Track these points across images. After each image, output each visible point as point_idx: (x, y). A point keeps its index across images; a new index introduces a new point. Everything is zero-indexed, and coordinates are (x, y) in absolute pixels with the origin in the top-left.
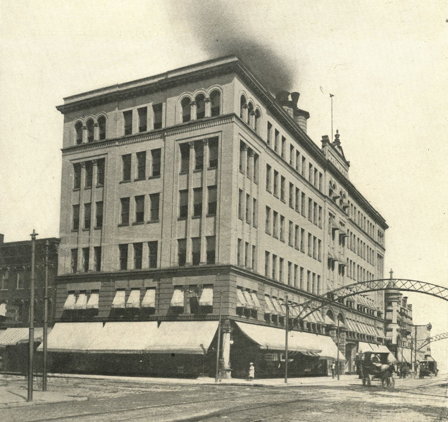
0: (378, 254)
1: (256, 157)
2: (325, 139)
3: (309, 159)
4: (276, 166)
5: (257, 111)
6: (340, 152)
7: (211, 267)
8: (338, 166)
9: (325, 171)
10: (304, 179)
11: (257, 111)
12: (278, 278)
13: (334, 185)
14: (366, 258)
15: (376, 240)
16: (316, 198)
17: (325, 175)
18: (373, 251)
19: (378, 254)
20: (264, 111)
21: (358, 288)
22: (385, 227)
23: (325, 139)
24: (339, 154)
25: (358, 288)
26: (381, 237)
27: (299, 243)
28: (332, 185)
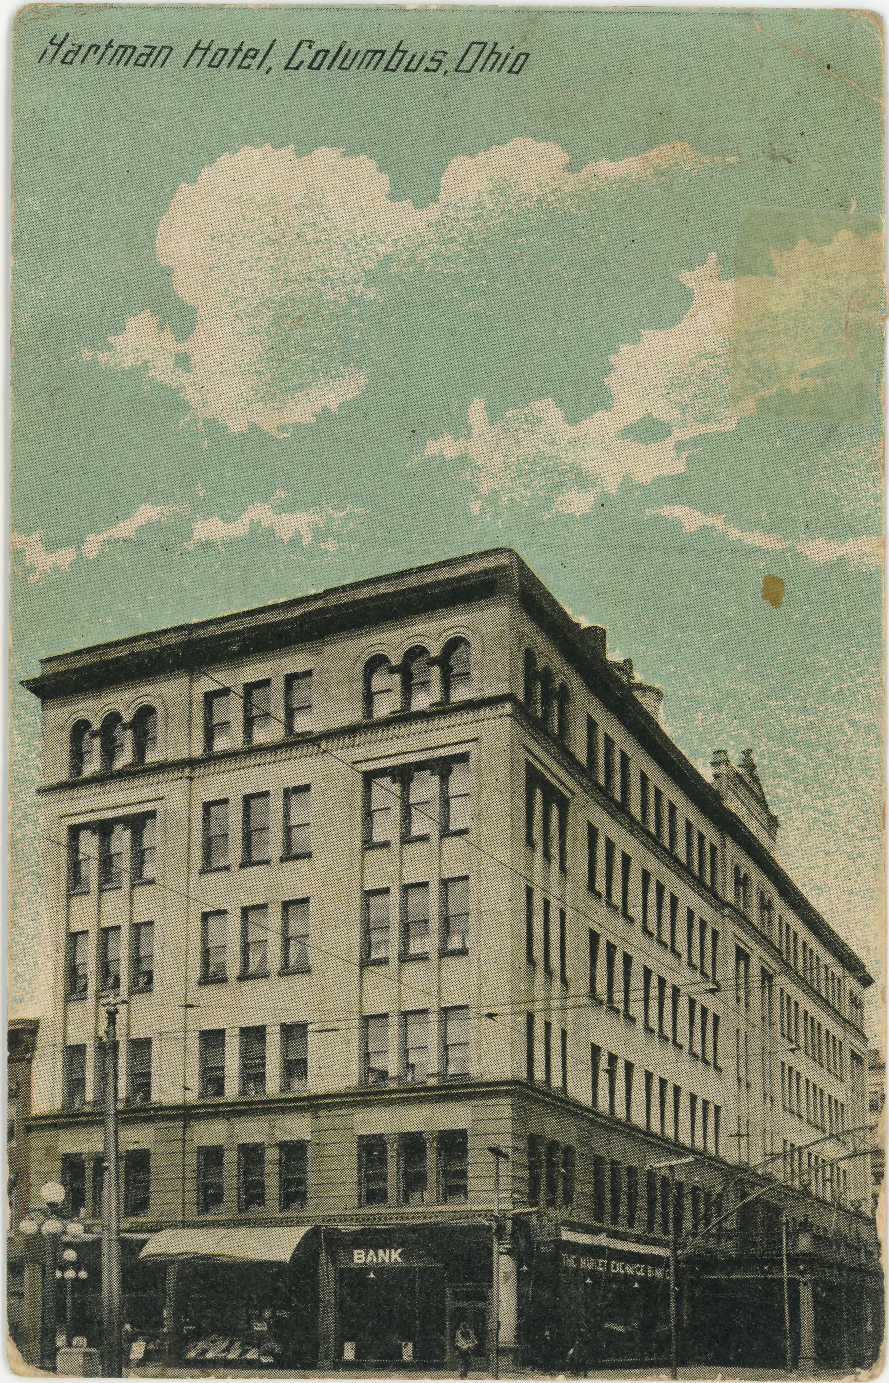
0: (853, 1053)
1: (564, 805)
2: (720, 757)
3: (686, 811)
4: (609, 828)
5: (563, 687)
6: (757, 792)
7: (116, 1077)
8: (753, 826)
9: (723, 837)
10: (676, 860)
11: (563, 687)
12: (670, 1132)
13: (745, 875)
14: (825, 1063)
15: (847, 1016)
16: (704, 910)
17: (724, 846)
18: (842, 1105)
19: (853, 1053)
20: (576, 685)
21: (858, 1141)
22: (867, 981)
23: (720, 757)
24: (751, 792)
25: (858, 1141)
26: (857, 1007)
27: (619, 997)
28: (742, 876)
